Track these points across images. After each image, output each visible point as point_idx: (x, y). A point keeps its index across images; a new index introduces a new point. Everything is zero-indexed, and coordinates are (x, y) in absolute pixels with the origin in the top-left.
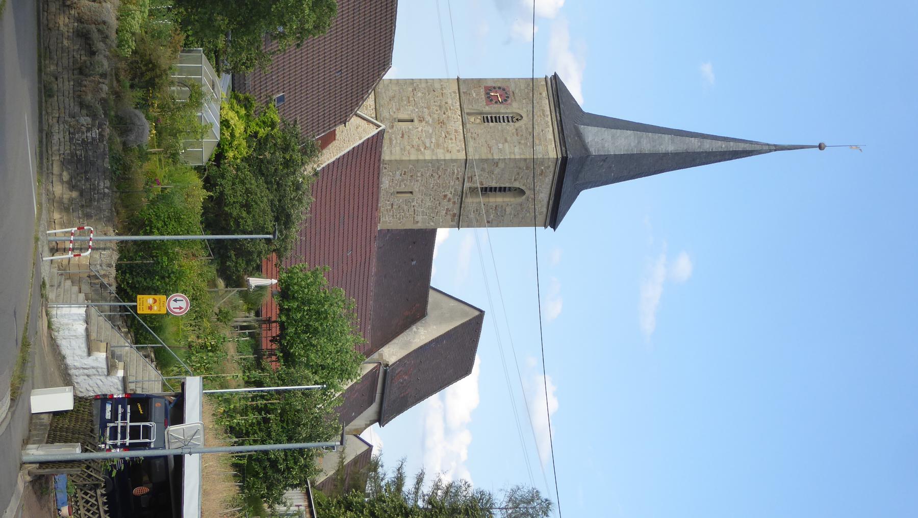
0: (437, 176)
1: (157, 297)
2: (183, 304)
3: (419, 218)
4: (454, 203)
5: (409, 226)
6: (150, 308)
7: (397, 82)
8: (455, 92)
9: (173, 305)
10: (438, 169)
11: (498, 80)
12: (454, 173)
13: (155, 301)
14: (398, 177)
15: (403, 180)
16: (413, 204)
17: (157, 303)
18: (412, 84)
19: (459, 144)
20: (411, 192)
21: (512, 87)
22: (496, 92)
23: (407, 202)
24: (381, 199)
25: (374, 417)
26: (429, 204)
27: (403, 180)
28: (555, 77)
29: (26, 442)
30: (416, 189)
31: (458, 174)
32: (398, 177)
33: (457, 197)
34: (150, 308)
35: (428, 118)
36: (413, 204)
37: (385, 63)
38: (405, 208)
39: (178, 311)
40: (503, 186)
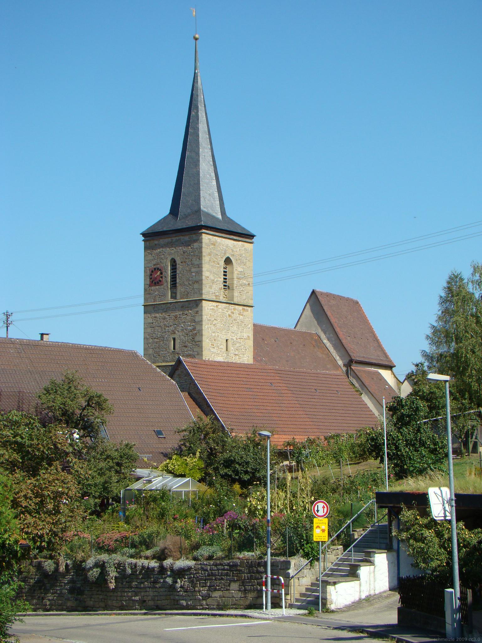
0: (215, 322)
1: (315, 525)
2: (321, 505)
3: (245, 335)
4: (234, 309)
5: (251, 343)
6: (323, 531)
7: (145, 349)
8: (154, 308)
9: (321, 513)
10: (209, 320)
11: (145, 272)
12: (213, 309)
13: (318, 527)
14: (215, 350)
15: (218, 347)
16: (235, 339)
17: (320, 525)
18: (147, 339)
19: (191, 305)
20: (227, 340)
21: (151, 266)
22: (153, 278)
23: (234, 344)
24: (230, 361)
25: (389, 372)
26: (235, 328)
27: (218, 347)
28: (144, 234)
29: (444, 635)
30: (225, 337)
31: (214, 306)
32: (215, 350)
33: (230, 307)
34: (323, 531)
35: (172, 328)
36: (235, 339)
37: (133, 355)
38: (238, 345)
39: (316, 509)
40: (223, 273)
